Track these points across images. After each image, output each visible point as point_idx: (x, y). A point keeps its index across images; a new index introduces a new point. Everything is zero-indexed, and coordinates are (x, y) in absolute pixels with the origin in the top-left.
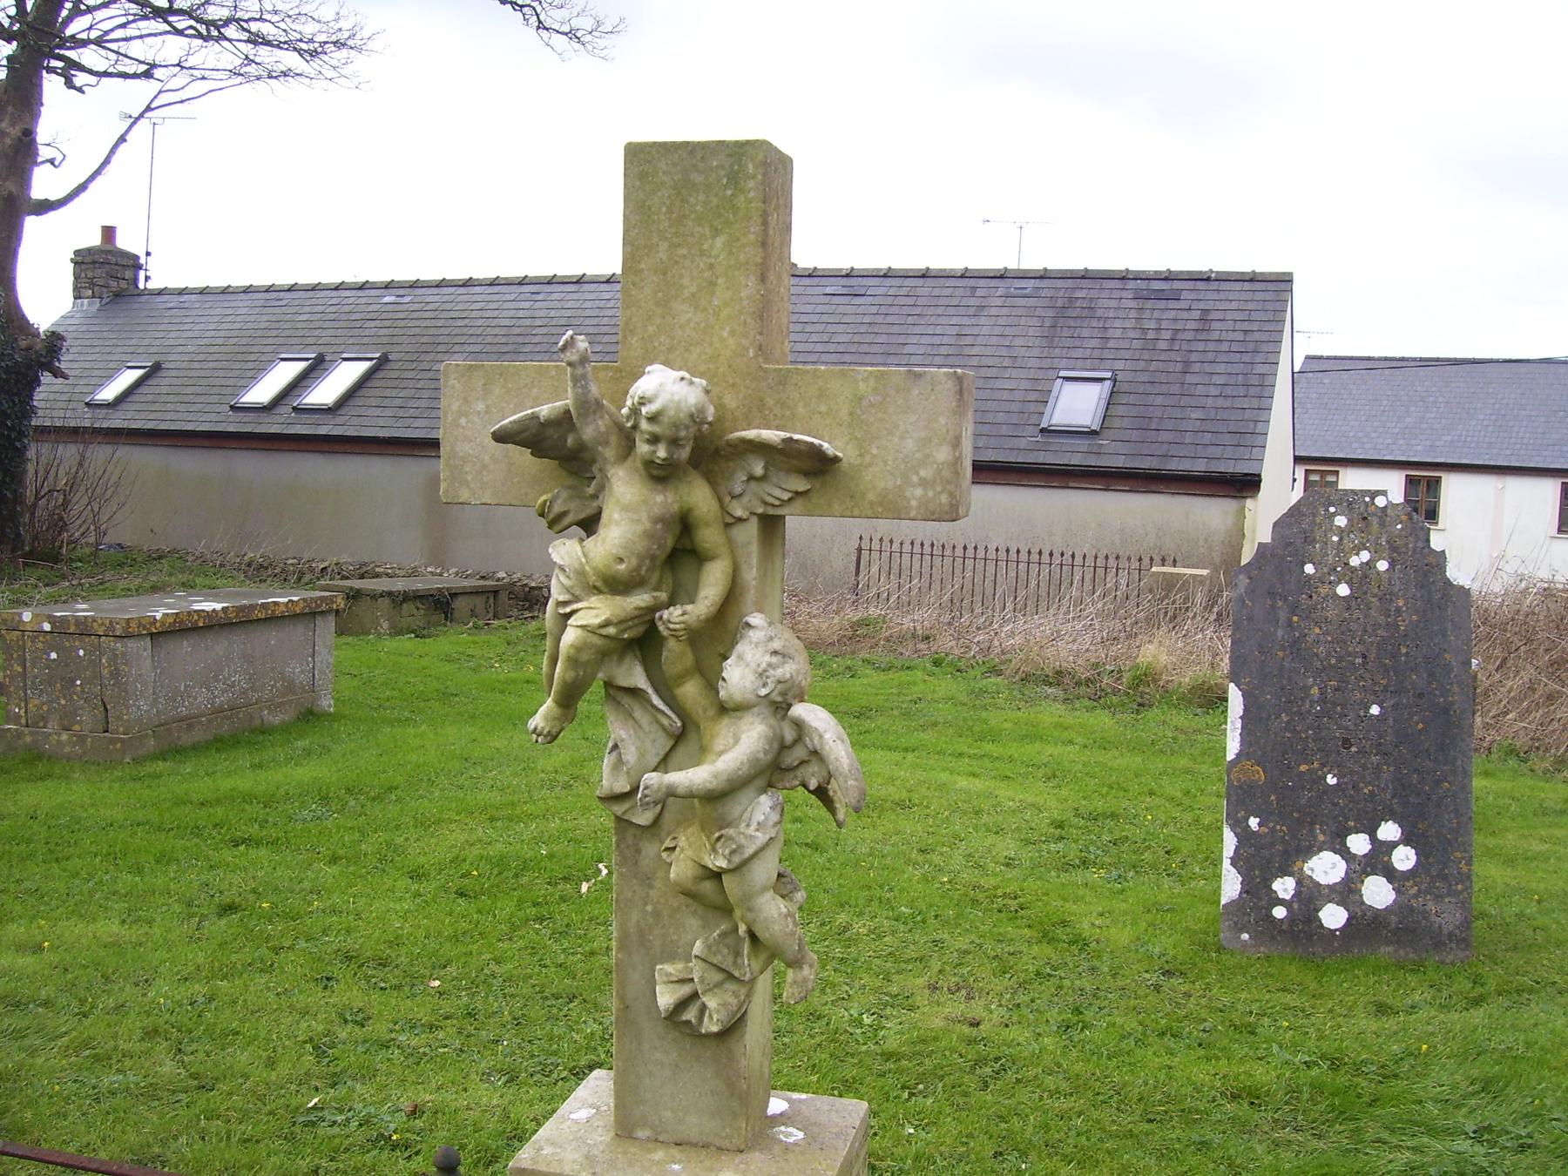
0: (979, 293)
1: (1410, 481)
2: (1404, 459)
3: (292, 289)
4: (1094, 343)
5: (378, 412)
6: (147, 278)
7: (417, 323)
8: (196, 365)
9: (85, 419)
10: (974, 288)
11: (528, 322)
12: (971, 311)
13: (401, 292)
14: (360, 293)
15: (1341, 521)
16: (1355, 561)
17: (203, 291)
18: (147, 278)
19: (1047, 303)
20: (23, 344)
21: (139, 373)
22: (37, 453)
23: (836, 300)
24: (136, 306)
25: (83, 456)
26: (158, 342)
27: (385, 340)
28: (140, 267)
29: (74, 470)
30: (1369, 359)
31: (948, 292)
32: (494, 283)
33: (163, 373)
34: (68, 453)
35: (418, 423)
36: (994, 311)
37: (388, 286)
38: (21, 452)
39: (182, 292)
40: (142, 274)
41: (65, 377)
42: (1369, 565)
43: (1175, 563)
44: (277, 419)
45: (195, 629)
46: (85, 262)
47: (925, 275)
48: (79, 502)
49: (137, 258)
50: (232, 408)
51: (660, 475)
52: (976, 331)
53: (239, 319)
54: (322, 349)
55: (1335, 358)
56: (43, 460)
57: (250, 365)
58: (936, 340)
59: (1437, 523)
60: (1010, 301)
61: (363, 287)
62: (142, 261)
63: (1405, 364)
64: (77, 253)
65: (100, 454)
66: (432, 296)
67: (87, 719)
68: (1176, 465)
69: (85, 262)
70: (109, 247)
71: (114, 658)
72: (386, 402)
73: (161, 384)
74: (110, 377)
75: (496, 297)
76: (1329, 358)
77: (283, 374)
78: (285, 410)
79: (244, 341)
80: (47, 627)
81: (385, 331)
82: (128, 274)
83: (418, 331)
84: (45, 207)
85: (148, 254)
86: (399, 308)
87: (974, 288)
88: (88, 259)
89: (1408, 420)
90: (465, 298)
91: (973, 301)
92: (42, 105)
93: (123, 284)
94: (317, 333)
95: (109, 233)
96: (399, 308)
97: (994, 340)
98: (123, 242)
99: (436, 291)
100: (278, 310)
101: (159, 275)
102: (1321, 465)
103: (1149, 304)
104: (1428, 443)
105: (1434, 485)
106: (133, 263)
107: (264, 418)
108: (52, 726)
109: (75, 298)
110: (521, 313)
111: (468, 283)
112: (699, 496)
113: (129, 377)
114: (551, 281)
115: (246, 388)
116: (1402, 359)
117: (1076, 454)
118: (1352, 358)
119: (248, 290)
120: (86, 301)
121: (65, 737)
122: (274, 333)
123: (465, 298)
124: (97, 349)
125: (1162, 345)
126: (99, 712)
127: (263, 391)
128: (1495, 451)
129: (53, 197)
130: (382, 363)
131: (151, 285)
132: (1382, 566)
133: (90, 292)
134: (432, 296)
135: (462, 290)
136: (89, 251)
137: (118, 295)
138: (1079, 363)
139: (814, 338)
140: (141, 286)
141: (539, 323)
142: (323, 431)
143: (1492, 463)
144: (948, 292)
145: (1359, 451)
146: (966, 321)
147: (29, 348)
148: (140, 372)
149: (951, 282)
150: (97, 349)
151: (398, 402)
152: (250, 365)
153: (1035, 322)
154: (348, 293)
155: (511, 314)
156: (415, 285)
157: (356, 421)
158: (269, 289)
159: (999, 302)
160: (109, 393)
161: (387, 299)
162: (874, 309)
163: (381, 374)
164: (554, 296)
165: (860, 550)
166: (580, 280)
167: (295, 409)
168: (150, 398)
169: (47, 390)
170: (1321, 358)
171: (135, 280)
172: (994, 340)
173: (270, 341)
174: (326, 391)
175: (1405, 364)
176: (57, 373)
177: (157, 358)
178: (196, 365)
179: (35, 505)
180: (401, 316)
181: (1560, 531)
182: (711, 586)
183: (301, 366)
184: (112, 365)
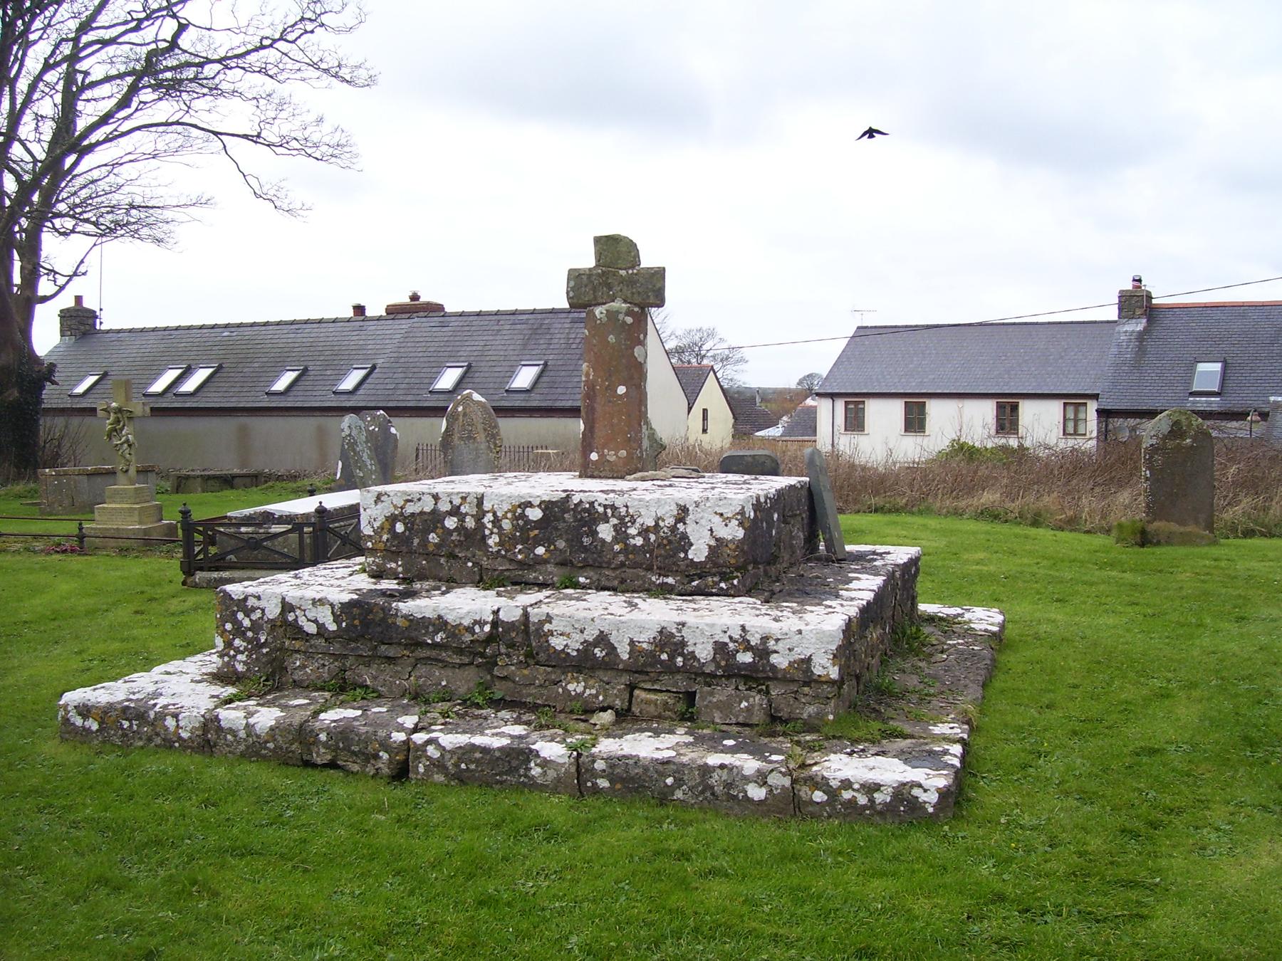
0: (502, 322)
1: (1000, 407)
2: (902, 391)
3: (177, 328)
4: (544, 346)
5: (214, 394)
6: (101, 323)
7: (239, 347)
8: (126, 373)
9: (266, 402)
10: (499, 321)
11: (291, 345)
12: (494, 333)
13: (233, 330)
14: (212, 331)
15: (369, 419)
16: (371, 429)
17: (131, 331)
18: (101, 323)
19: (530, 327)
20: (37, 369)
21: (96, 378)
22: (45, 423)
23: (434, 329)
24: (95, 340)
25: (67, 422)
26: (106, 360)
27: (222, 356)
28: (97, 317)
29: (63, 429)
30: (896, 327)
31: (486, 323)
32: (278, 323)
33: (109, 378)
34: (60, 421)
35: (233, 399)
36: (504, 332)
37: (227, 326)
38: (37, 421)
39: (119, 331)
40: (98, 321)
41: (58, 384)
42: (374, 430)
43: (546, 449)
44: (165, 400)
45: (102, 474)
46: (65, 315)
47: (479, 314)
48: (66, 444)
49: (95, 312)
50: (144, 395)
51: (115, 413)
52: (493, 343)
53: (150, 346)
54: (191, 362)
55: (876, 327)
56: (48, 425)
57: (154, 372)
58: (474, 348)
59: (924, 432)
60: (514, 327)
61: (214, 327)
62: (98, 314)
63: (901, 329)
64: (61, 311)
65: (75, 421)
66: (248, 331)
67: (66, 502)
68: (559, 404)
69: (65, 315)
70: (78, 308)
71: (75, 482)
72: (220, 389)
73: (108, 383)
74: (81, 380)
75: (278, 332)
76: (872, 327)
77: (171, 376)
78: (170, 395)
79: (151, 359)
80: (54, 473)
81: (223, 352)
82: (90, 321)
83: (238, 351)
84: (45, 299)
85: (101, 310)
86: (231, 338)
87: (499, 321)
88: (67, 315)
89: (911, 366)
90: (264, 332)
91: (497, 328)
92: (41, 250)
93: (87, 327)
94: (188, 353)
95: (79, 299)
96: (231, 338)
97: (500, 347)
98: (87, 304)
99: (249, 329)
100: (170, 341)
101: (108, 322)
102: (1076, 399)
103: (576, 325)
104: (920, 380)
105: (1015, 408)
106: (92, 315)
107: (160, 399)
108: (56, 505)
109: (62, 336)
110: (290, 341)
111: (266, 324)
112: (119, 415)
113: (91, 380)
114: (306, 322)
115: (151, 384)
116: (916, 326)
117: (517, 402)
118: (885, 327)
119: (154, 330)
120: (67, 338)
121: (60, 508)
122: (167, 354)
123: (264, 332)
124: (74, 365)
125: (574, 346)
126: (71, 500)
127: (159, 386)
128: (958, 384)
129: (48, 294)
130: (220, 368)
131: (104, 327)
132: (377, 429)
133: (69, 333)
134: (248, 331)
135: (264, 328)
136: (68, 310)
137: (85, 334)
138: (534, 357)
139: (420, 349)
140: (98, 327)
141: (297, 345)
142: (187, 405)
143: (955, 392)
144: (486, 323)
145: (1021, 388)
146: (491, 338)
147: (39, 371)
148: (97, 377)
149: (490, 317)
150: (74, 365)
151: (225, 389)
152: (154, 372)
153: (522, 337)
154: (205, 331)
155: (285, 341)
156: (240, 325)
157: (204, 399)
158: (166, 329)
159: (508, 327)
160: (80, 389)
161: (226, 334)
162: (450, 334)
163: (218, 375)
164: (306, 331)
165: (417, 449)
166: (320, 321)
167: (175, 394)
168: (102, 391)
169: (50, 395)
170: (866, 327)
171: (95, 324)
172: (500, 347)
173: (165, 358)
174: (190, 385)
175: (901, 329)
176: (54, 383)
177: (105, 369)
178: (126, 373)
179: (44, 446)
180: (231, 343)
181: (906, 431)
182: (121, 424)
183: (179, 371)
184: (82, 374)
